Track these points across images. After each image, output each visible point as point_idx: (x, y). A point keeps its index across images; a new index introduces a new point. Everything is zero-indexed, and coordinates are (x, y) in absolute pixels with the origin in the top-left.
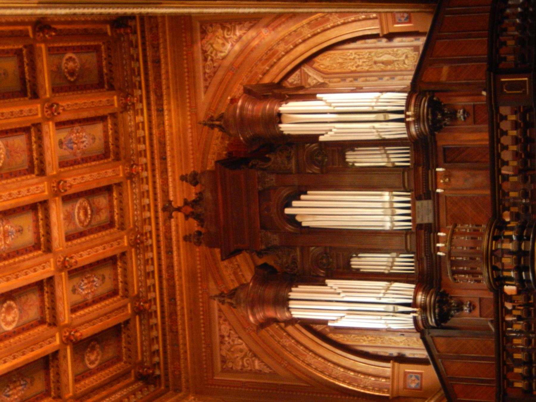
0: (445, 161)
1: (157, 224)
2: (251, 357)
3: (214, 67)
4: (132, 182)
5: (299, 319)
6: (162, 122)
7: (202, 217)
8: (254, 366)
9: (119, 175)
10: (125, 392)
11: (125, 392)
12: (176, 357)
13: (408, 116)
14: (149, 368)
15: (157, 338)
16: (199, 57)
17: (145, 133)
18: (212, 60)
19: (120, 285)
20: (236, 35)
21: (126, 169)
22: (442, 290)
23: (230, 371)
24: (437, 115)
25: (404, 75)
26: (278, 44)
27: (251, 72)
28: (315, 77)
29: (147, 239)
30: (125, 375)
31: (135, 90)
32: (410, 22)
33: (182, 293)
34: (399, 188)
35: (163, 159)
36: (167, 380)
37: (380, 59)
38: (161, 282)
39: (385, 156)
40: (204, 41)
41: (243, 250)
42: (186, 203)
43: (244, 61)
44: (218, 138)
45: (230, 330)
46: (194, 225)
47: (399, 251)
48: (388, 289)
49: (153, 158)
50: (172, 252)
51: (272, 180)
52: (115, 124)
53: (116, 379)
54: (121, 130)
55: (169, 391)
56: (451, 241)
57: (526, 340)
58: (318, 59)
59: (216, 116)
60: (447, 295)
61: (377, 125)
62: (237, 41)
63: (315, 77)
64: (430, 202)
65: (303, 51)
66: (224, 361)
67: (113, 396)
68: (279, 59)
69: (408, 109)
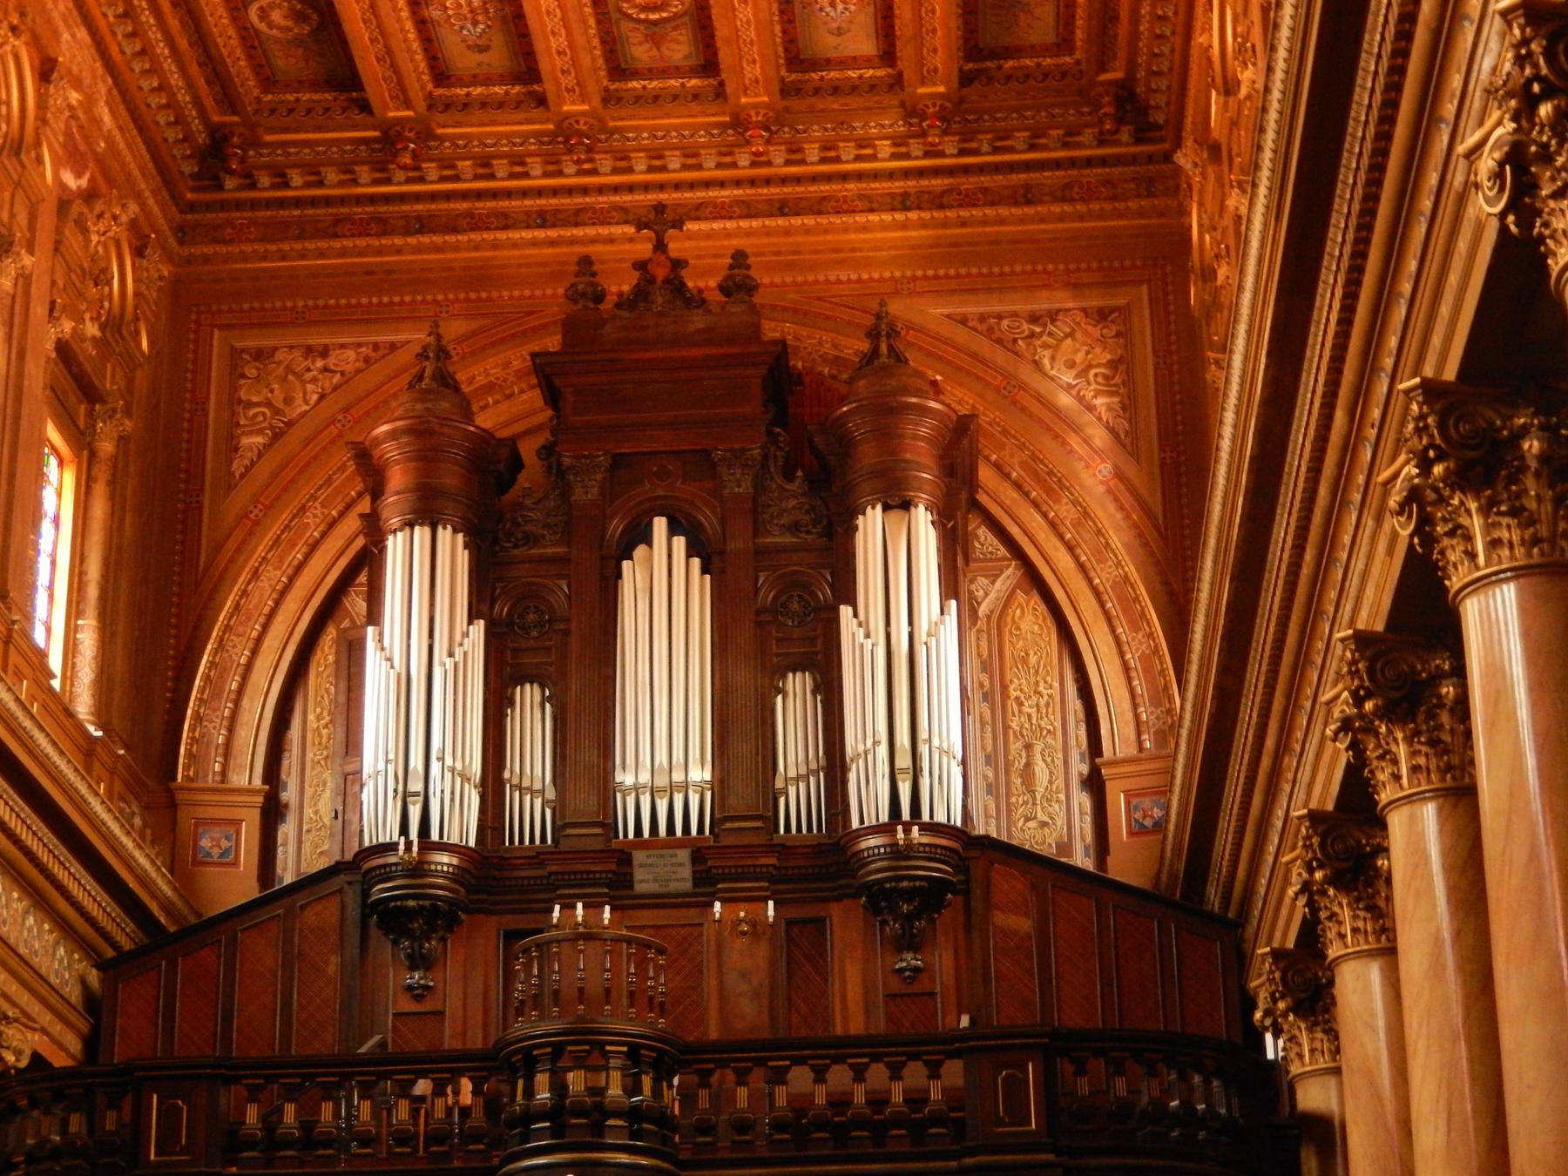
0: (790, 923)
1: (616, 189)
2: (272, 428)
3: (1015, 340)
4: (723, 126)
5: (383, 550)
6: (875, 205)
7: (642, 305)
8: (251, 433)
9: (746, 95)
10: (183, 97)
11: (183, 97)
12: (272, 232)
13: (907, 831)
14: (242, 160)
15: (320, 184)
17: (848, 162)
18: (1032, 335)
19: (461, 92)
20: (1095, 397)
21: (757, 114)
22: (463, 917)
23: (235, 371)
24: (909, 901)
25: (998, 819)
26: (1075, 503)
27: (1005, 432)
28: (992, 595)
29: (578, 162)
30: (229, 100)
31: (956, 138)
32: (1131, 833)
33: (437, 249)
34: (722, 806)
35: (783, 208)
36: (208, 207)
37: (1038, 758)
38: (465, 195)
39: (803, 771)
40: (1080, 317)
41: (556, 408)
42: (678, 264)
43: (1031, 415)
44: (836, 347)
45: (342, 373)
46: (621, 284)
47: (559, 807)
48: (466, 779)
49: (784, 181)
50: (782, 213)
51: (739, 484)
52: (873, 87)
53: (217, 75)
54: (856, 102)
55: (181, 212)
56: (589, 935)
57: (331, 1133)
58: (1036, 599)
59: (900, 346)
60: (450, 929)
61: (883, 751)
62: (1081, 399)
63: (992, 595)
64: (687, 886)
65: (1058, 564)
66: (260, 355)
67: (174, 68)
68: (1035, 504)
69: (925, 828)
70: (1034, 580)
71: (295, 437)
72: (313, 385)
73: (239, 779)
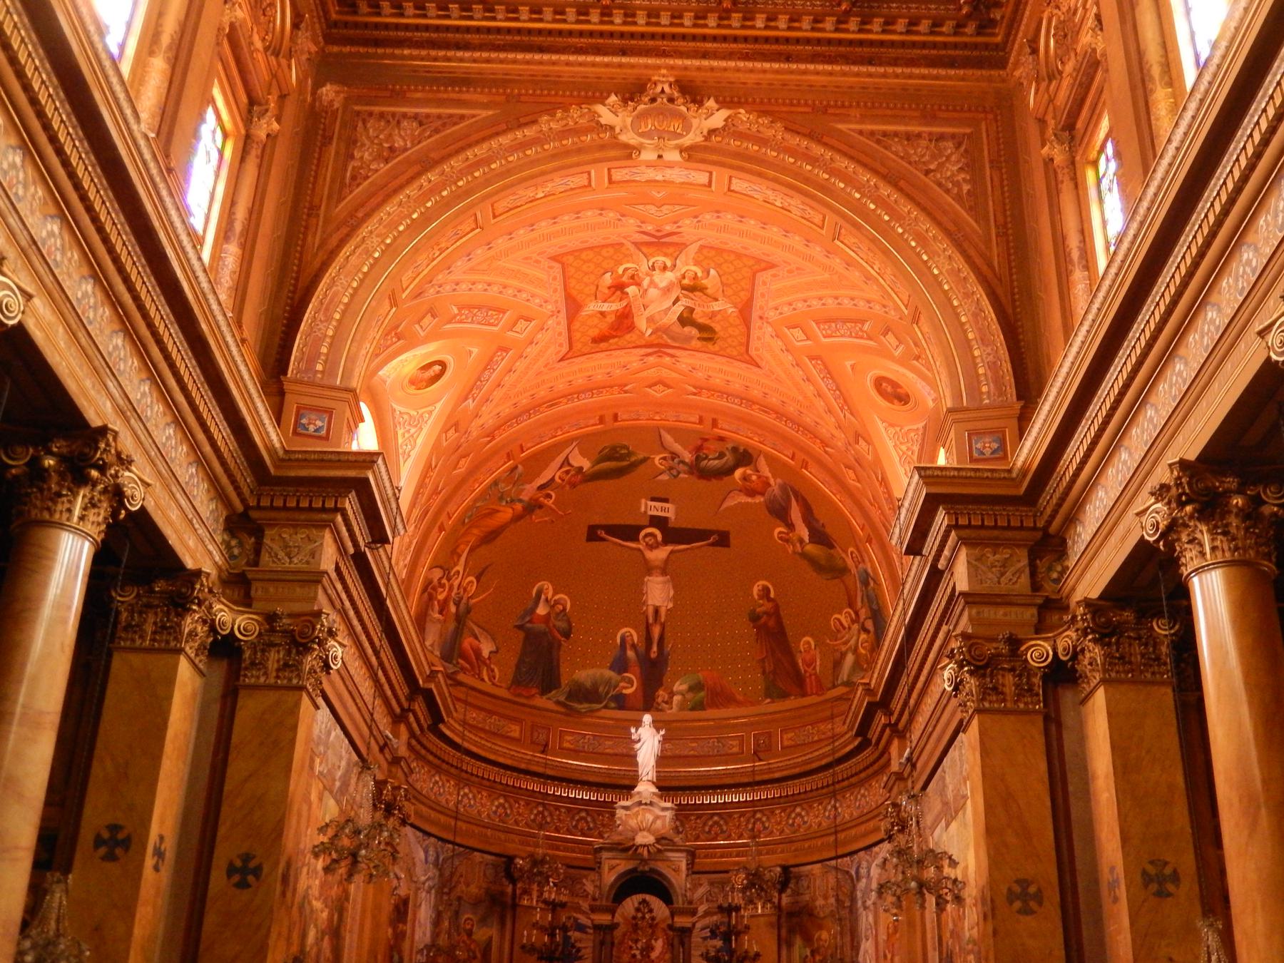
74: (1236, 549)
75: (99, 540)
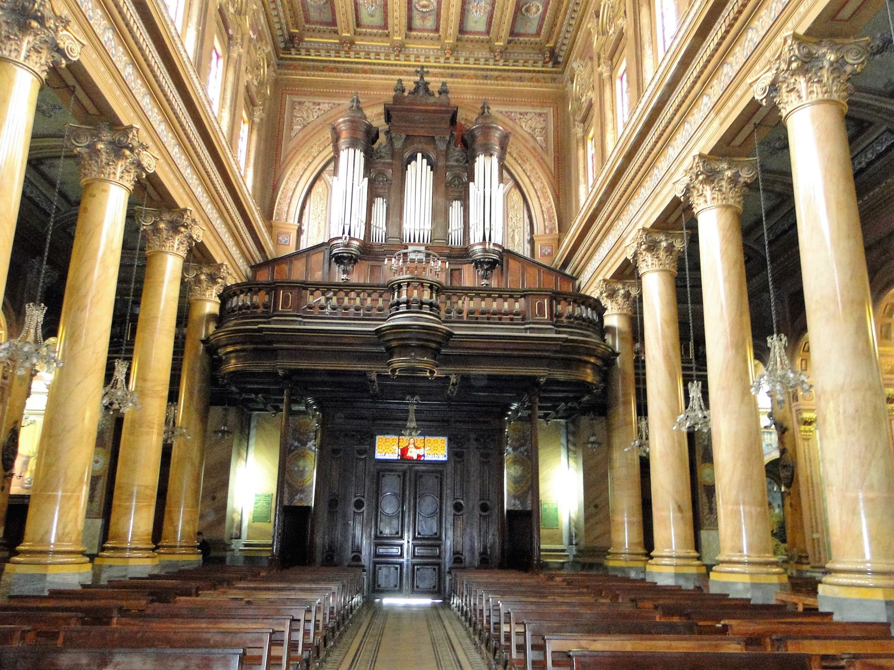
0: (452, 270)
16: (523, 110)
19: (364, 30)
51: (442, 146)
58: (517, 191)
66: (300, 103)
70: (517, 185)
71: (310, 127)
72: (317, 114)
73: (291, 221)
74: (826, 92)
75: (131, 188)
